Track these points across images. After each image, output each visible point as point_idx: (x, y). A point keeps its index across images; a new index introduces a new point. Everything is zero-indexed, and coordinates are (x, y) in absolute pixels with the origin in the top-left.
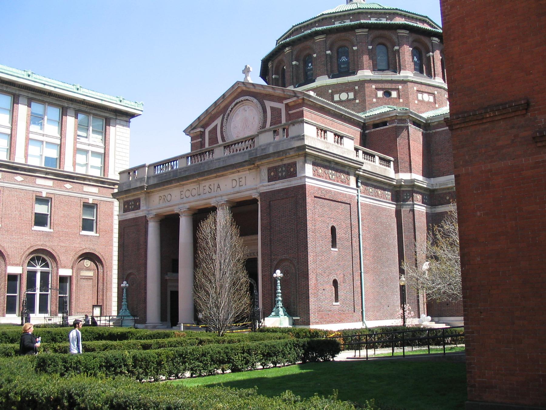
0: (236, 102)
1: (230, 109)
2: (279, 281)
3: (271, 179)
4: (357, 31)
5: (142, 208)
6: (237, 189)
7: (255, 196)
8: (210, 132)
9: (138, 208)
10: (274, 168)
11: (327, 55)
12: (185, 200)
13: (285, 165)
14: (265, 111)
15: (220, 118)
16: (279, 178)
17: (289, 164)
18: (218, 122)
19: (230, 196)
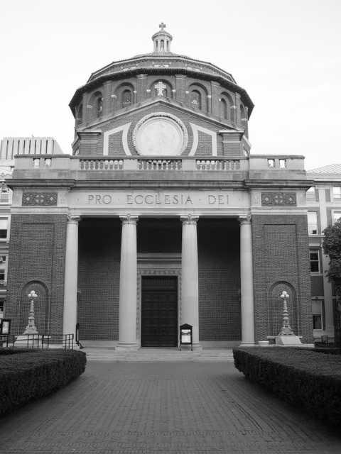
0: (152, 114)
1: (143, 119)
2: (285, 302)
3: (264, 204)
4: (212, 82)
5: (59, 205)
6: (216, 206)
7: (242, 215)
8: (111, 137)
9: (55, 203)
10: (269, 194)
11: (186, 95)
12: (135, 206)
13: (282, 193)
14: (190, 133)
15: (129, 124)
16: (276, 204)
17: (288, 194)
18: (125, 128)
19: (84, 211)
